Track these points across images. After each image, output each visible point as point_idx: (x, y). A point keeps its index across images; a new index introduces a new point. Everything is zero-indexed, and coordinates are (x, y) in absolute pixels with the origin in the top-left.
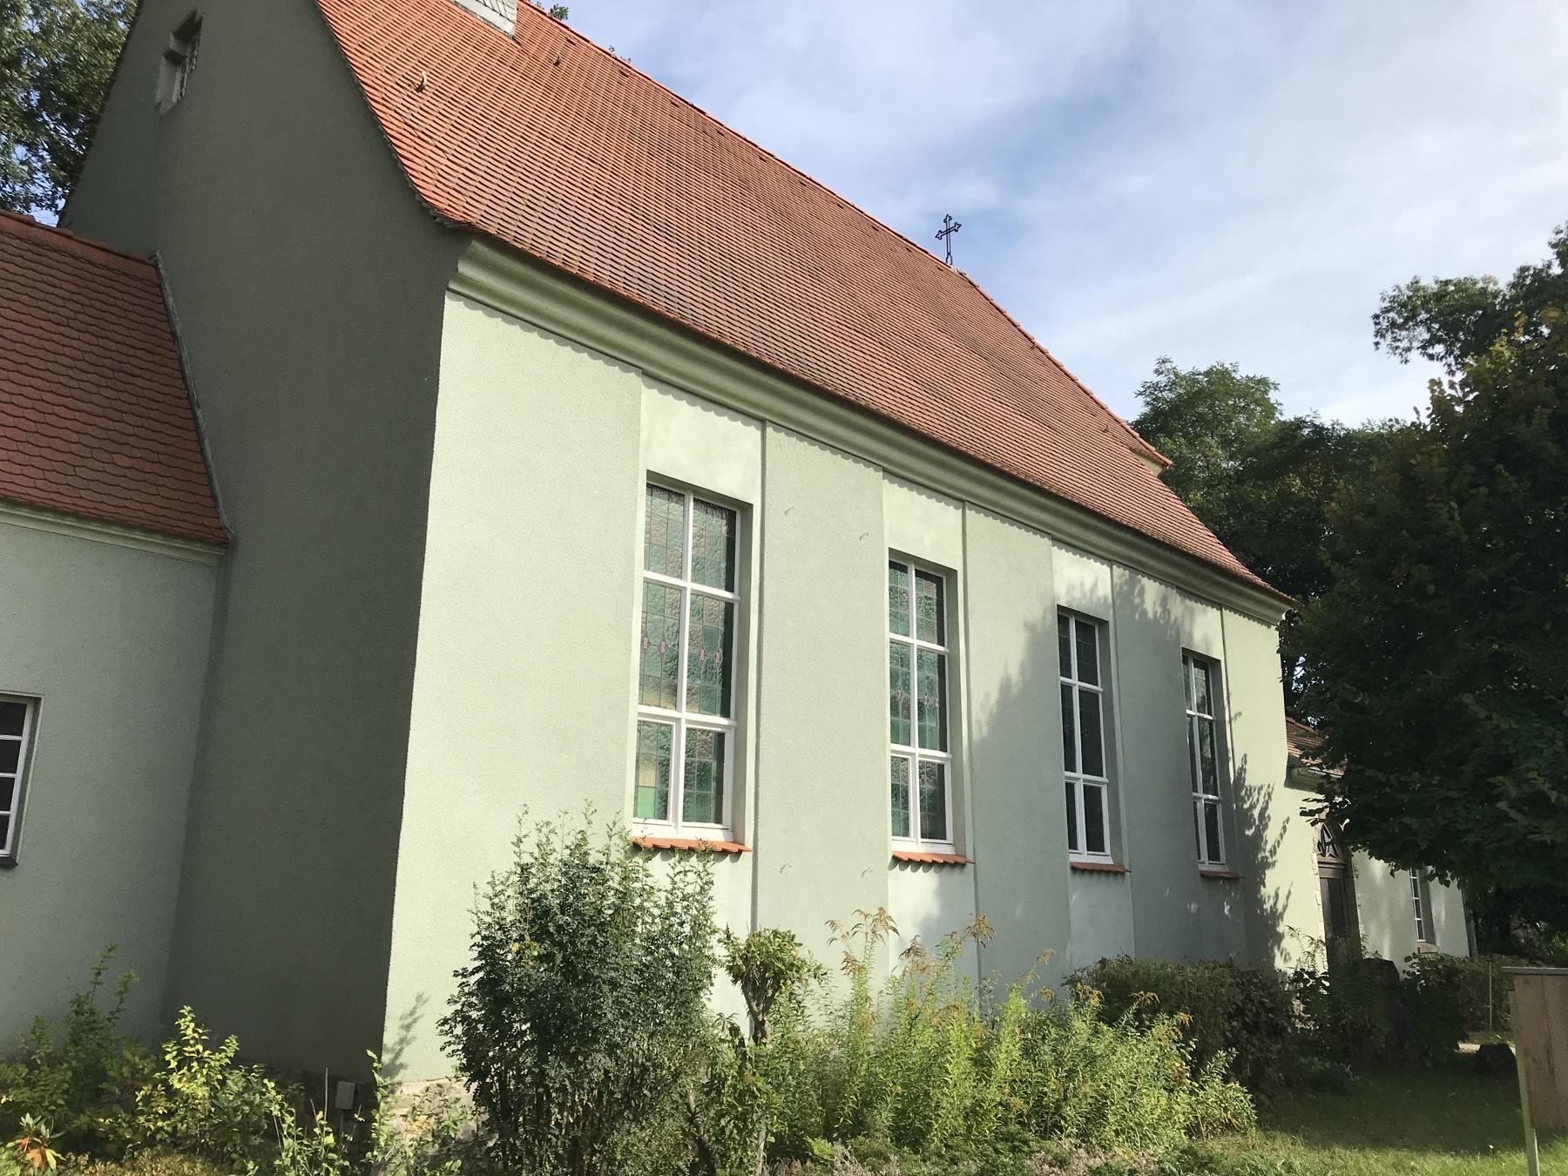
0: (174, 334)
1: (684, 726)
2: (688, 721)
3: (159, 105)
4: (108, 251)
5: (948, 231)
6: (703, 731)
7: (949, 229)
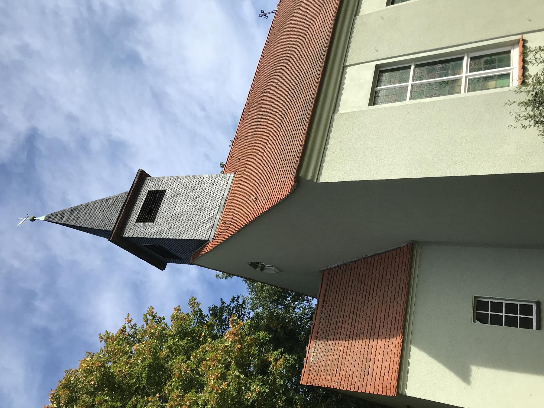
0: (344, 264)
1: (469, 74)
2: (466, 73)
3: (277, 272)
4: (322, 284)
5: (264, 14)
6: (470, 66)
7: (263, 14)
